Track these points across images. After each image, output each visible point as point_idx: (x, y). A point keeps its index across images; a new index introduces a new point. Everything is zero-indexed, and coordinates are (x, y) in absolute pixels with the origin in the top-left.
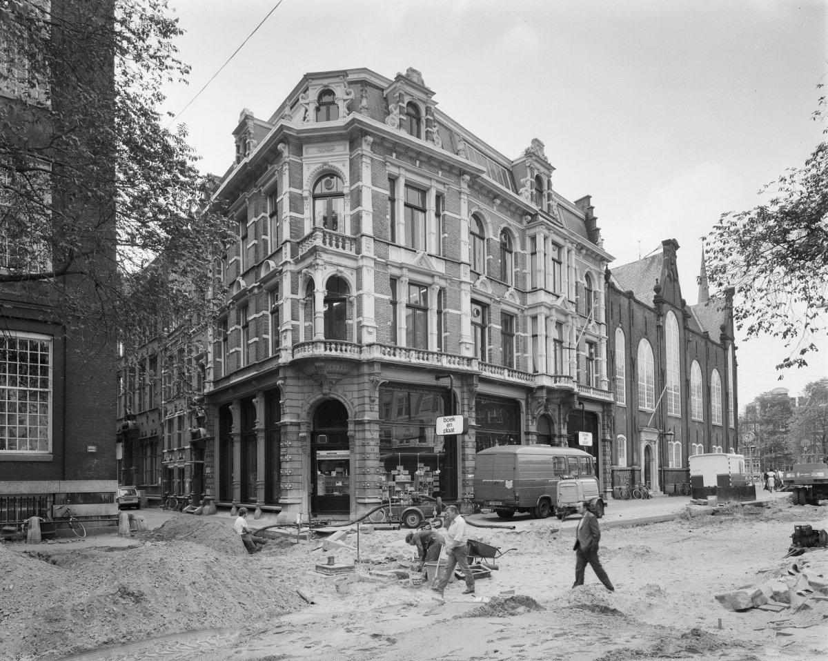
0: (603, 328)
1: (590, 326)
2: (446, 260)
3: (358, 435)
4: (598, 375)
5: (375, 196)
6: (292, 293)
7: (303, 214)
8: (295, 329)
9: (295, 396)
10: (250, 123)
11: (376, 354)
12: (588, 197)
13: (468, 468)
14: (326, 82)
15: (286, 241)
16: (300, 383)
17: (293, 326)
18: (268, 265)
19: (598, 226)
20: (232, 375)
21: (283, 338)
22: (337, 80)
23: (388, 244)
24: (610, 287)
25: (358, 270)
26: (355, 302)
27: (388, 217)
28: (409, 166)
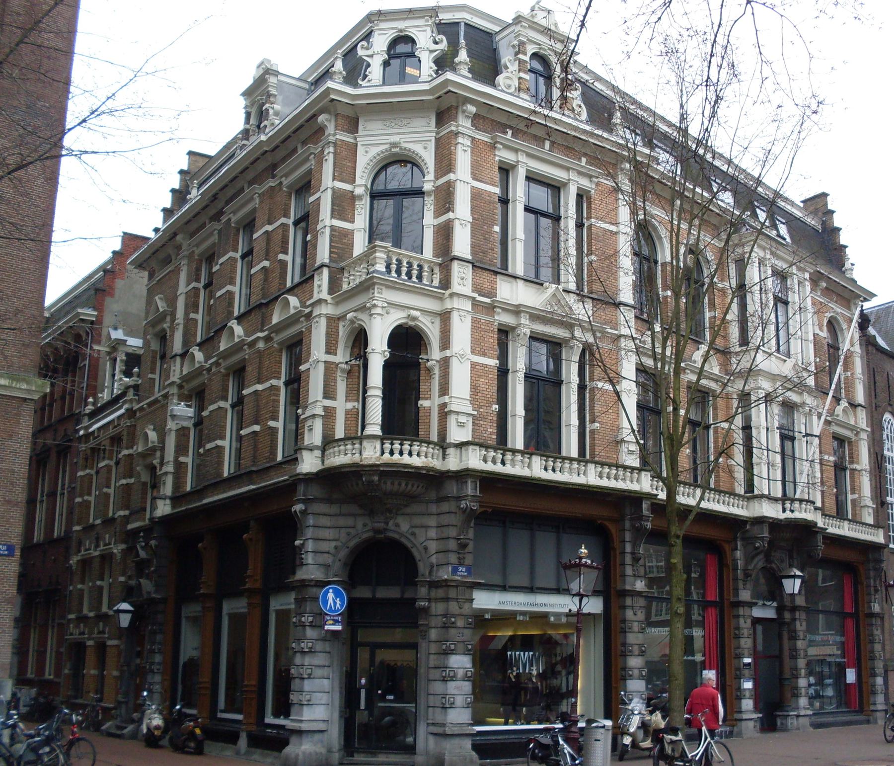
0: (862, 415)
1: (839, 410)
2: (593, 299)
3: (438, 608)
4: (856, 496)
5: (476, 196)
6: (328, 352)
7: (353, 222)
8: (329, 415)
9: (325, 521)
10: (272, 80)
11: (475, 460)
12: (824, 195)
13: (632, 645)
14: (401, 25)
15: (322, 266)
16: (334, 509)
17: (326, 408)
18: (287, 303)
19: (843, 241)
20: (206, 487)
21: (306, 429)
22: (421, 22)
23: (496, 273)
24: (868, 342)
25: (445, 317)
26: (437, 371)
27: (497, 229)
28: (533, 148)
